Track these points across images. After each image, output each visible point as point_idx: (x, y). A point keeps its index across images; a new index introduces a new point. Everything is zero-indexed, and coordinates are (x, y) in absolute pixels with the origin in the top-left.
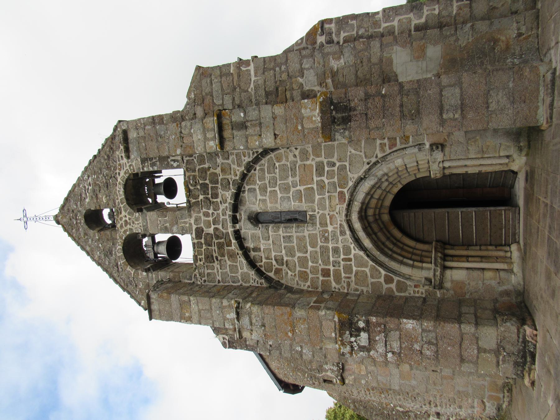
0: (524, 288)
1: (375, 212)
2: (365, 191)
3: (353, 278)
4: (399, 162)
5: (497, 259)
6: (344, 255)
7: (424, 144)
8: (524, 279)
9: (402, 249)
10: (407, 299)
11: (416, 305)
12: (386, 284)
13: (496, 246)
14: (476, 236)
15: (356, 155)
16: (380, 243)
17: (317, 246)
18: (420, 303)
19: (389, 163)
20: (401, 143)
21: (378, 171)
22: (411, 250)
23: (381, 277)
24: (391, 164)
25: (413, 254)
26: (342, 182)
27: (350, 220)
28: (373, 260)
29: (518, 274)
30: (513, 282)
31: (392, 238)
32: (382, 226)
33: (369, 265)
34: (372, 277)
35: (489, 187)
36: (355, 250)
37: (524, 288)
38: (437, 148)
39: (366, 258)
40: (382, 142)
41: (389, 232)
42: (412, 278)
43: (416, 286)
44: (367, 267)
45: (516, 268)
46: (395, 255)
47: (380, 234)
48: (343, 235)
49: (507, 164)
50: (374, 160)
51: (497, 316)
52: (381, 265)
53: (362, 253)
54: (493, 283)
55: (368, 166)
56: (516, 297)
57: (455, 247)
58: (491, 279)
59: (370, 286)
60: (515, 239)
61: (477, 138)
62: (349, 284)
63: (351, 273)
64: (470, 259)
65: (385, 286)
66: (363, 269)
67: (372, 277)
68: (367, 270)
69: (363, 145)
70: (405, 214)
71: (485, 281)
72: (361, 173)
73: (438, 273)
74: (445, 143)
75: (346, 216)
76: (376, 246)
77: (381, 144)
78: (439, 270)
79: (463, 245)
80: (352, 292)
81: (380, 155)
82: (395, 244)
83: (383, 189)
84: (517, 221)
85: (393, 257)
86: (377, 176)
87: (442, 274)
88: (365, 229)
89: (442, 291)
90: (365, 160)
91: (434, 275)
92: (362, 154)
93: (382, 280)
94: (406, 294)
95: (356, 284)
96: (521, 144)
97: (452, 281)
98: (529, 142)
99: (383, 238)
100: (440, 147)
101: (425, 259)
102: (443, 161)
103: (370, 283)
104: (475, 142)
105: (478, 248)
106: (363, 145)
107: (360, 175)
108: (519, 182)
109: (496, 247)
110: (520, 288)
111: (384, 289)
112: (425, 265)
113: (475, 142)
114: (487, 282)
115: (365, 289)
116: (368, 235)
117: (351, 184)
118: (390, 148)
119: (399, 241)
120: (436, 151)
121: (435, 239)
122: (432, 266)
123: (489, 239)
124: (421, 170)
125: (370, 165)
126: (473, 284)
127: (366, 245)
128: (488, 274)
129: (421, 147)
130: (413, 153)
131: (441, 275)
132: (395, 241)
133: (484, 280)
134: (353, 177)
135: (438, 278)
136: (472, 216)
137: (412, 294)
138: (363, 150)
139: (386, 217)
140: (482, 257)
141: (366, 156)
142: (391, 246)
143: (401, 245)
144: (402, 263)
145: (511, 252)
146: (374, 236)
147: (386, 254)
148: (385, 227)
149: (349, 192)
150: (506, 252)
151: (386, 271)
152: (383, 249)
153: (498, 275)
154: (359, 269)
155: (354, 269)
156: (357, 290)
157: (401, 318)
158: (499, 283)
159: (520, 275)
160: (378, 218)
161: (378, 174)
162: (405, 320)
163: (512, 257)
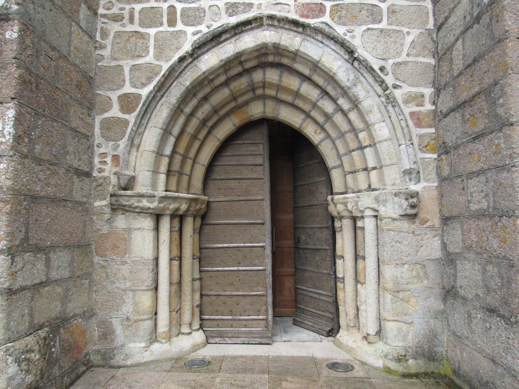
0: (119, 367)
1: (271, 85)
2: (323, 59)
3: (130, 28)
4: (382, 131)
5: (176, 311)
6: (183, 10)
7: (419, 181)
8: (138, 365)
9: (194, 137)
10: (88, 137)
11: (67, 153)
12: (119, 97)
13: (200, 306)
14: (218, 271)
15: (402, 45)
16: (207, 90)
17: (186, 24)
18: (73, 161)
19: (380, 111)
20: (421, 137)
21: (364, 88)
22: (192, 155)
23: (135, 86)
24: (379, 116)
25: (185, 157)
26: (344, 12)
27: (262, 25)
28: (172, 70)
29: (147, 354)
30: (132, 345)
31: (215, 118)
32: (241, 100)
33: (161, 63)
34: (134, 68)
35: (296, 288)
36: (194, 34)
37: (119, 367)
38: (413, 206)
39: (176, 58)
40: (427, 99)
41: (228, 114)
42: (134, 150)
43: (116, 158)
44: (157, 57)
45: (159, 349)
46: (181, 120)
47: (225, 93)
48: (227, 10)
49: (357, 326)
50: (390, 80)
51: (42, 333)
52: (162, 88)
53: (187, 47)
54: (127, 309)
55: (376, 68)
56: (99, 351)
57: (197, 236)
58: (136, 304)
59: (113, 63)
60: (213, 337)
61: (426, 282)
62: (117, 18)
63: (142, 24)
64: (176, 263)
65: (114, 96)
66: (152, 50)
67: (134, 68)
68: (150, 58)
69: (421, 59)
70: (261, 147)
71: (130, 294)
72: (361, 52)
73: (145, 203)
74: (417, 221)
75: (271, 17)
76: (204, 79)
77: (423, 96)
78: (151, 206)
79: (200, 248)
80: (99, 25)
81: (398, 94)
82: (204, 122)
83: (319, 104)
84: (246, 340)
85: (179, 116)
86: (355, 85)
87: (143, 212)
88: (238, 58)
89: (108, 210)
90: (391, 62)
91: (142, 196)
92: (403, 58)
93: (128, 89)
94: (98, 138)
95: (118, 34)
96: (411, 361)
97: (129, 230)
98: (416, 375)
99: (217, 98)
100: (413, 212)
101: (174, 180)
102: (376, 217)
103: (121, 63)
104: (418, 276)
105: (197, 276)
106: (421, 59)
107: (359, 51)
108: (315, 341)
109: (197, 307)
110: (118, 360)
111: (109, 94)
112: (162, 178)
113: (418, 276)
114: (128, 298)
115: (106, 52)
116: (226, 65)
117: (340, 30)
118: (412, 114)
119: (209, 132)
120: (405, 204)
121: (212, 200)
122: (160, 192)
123: (213, 293)
124: (349, 177)
125: (379, 72)
126: (125, 270)
127: (206, 57)
128: (145, 300)
129: (414, 175)
130: (400, 159)
131: (142, 208)
132: (210, 124)
133: (133, 291)
134: (357, 37)
135: (134, 202)
136: (255, 265)
137: (98, 151)
138: (410, 59)
139: (256, 110)
140: (180, 283)
141: (398, 65)
142: (201, 114)
143: (201, 136)
144: (166, 132)
145: (190, 334)
146: (223, 78)
147: (184, 100)
148: (239, 107)
149: (323, 26)
150: (190, 325)
151: (148, 97)
152: (195, 95)
153: (146, 317)
154: (152, 42)
155: (152, 31)
156: (104, 34)
157: (20, 105)
158: (128, 319)
159: (147, 357)
160: (257, 93)
161: (359, 87)
162: (11, 113)
163: (181, 336)
